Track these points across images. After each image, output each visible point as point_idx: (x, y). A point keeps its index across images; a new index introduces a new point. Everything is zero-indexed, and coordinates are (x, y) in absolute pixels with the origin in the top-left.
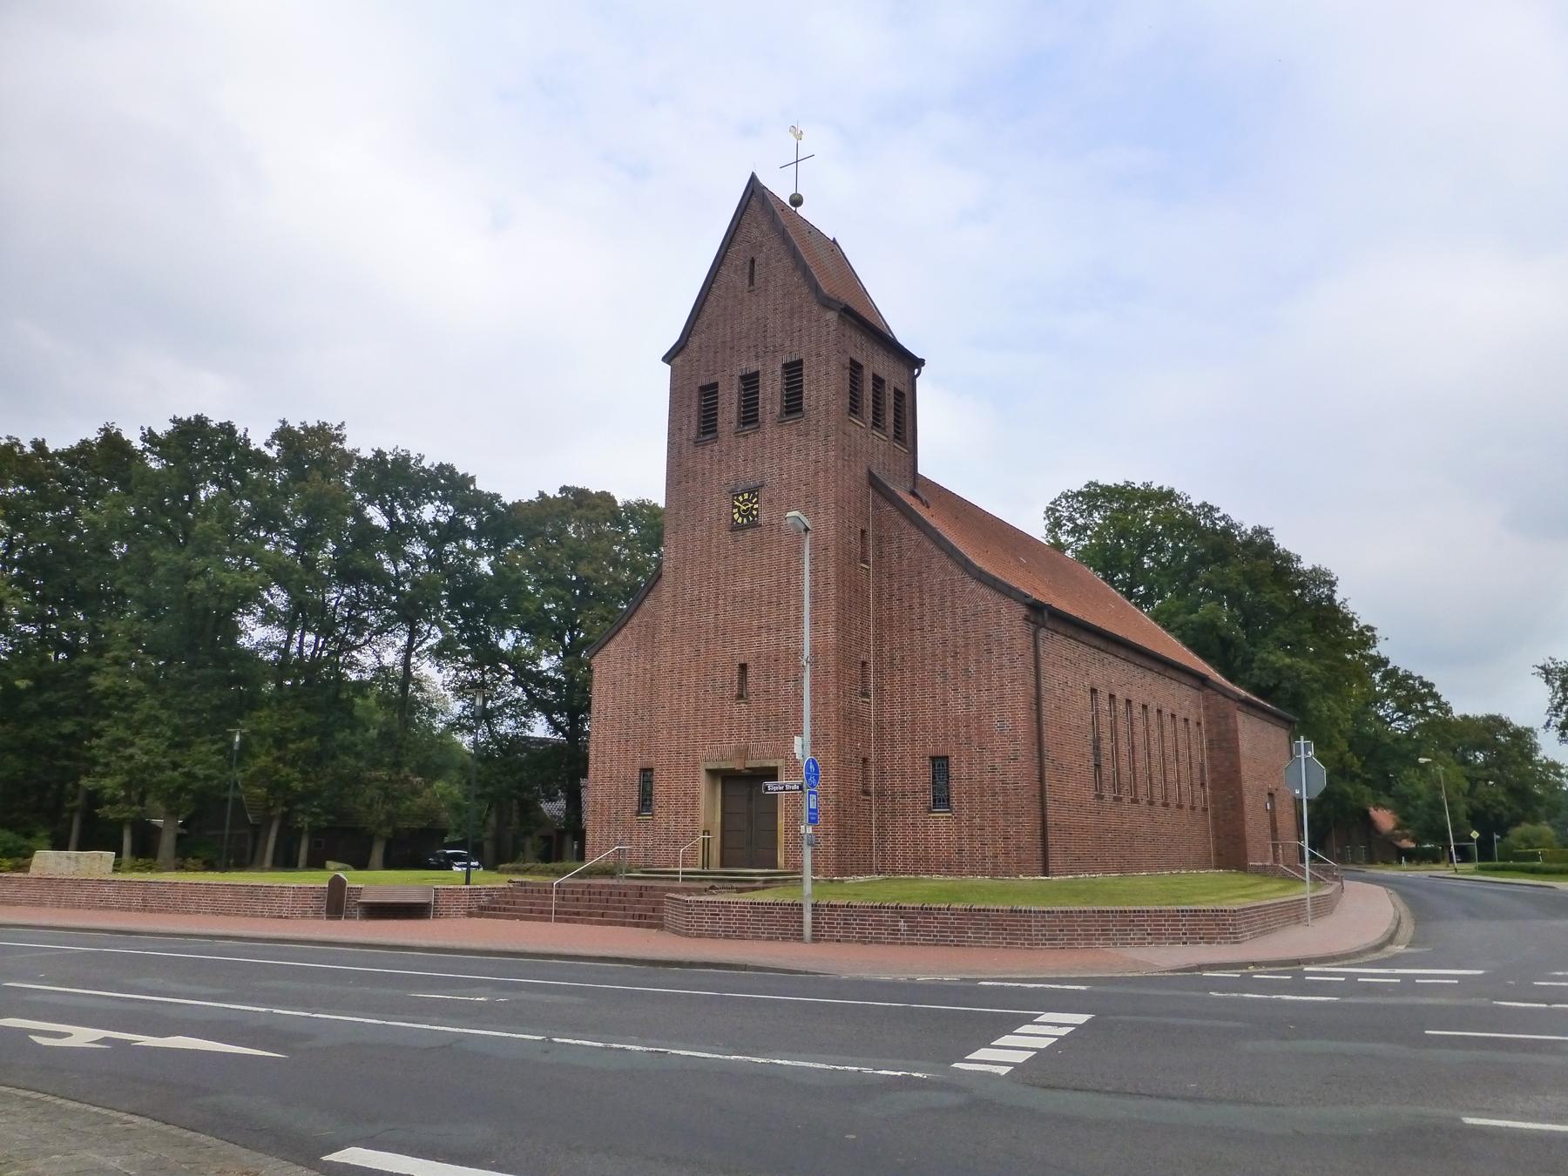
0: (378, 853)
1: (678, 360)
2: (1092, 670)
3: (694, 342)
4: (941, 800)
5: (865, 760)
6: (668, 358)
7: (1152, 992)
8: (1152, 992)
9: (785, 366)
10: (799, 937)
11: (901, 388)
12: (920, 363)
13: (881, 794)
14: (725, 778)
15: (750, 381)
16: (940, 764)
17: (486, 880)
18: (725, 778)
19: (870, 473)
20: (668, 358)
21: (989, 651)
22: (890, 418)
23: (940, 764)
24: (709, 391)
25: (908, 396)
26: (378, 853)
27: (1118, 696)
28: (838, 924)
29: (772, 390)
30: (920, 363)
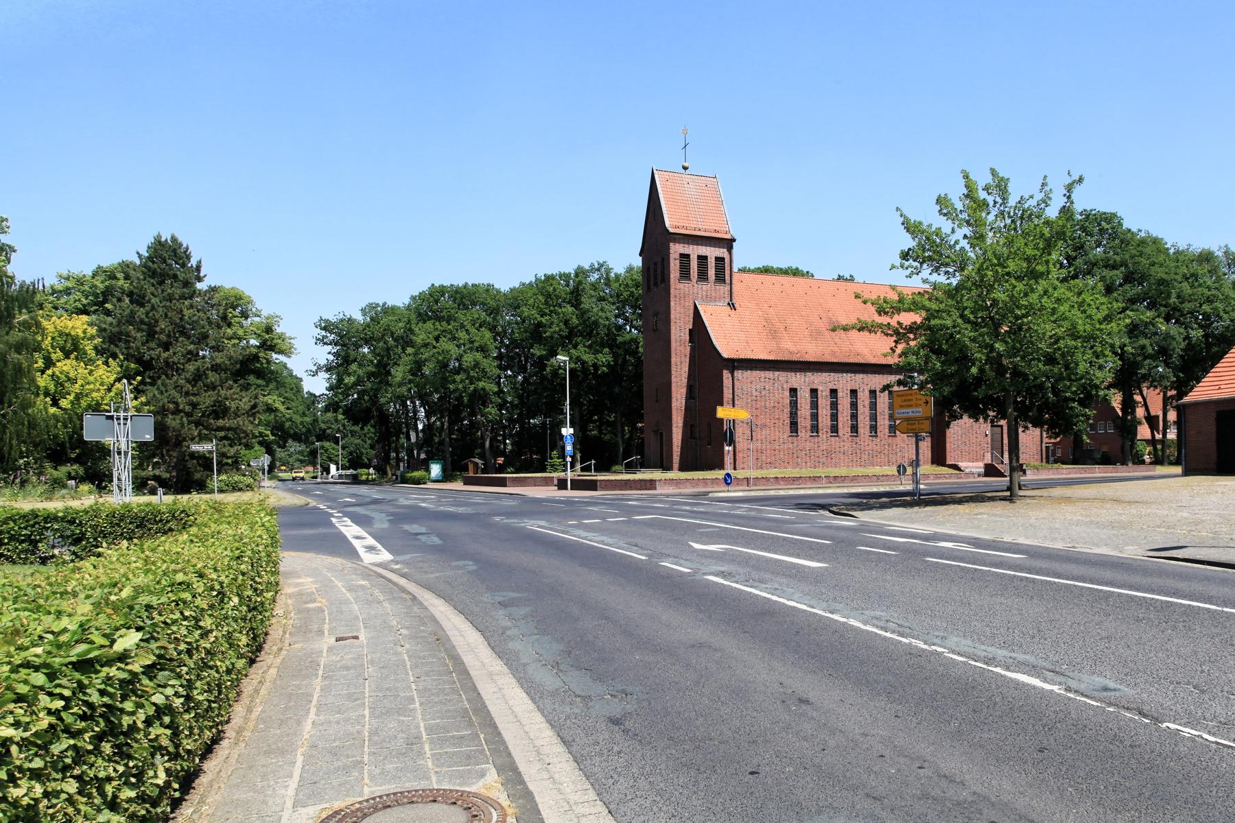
22: (712, 272)
25: (727, 261)
27: (820, 388)
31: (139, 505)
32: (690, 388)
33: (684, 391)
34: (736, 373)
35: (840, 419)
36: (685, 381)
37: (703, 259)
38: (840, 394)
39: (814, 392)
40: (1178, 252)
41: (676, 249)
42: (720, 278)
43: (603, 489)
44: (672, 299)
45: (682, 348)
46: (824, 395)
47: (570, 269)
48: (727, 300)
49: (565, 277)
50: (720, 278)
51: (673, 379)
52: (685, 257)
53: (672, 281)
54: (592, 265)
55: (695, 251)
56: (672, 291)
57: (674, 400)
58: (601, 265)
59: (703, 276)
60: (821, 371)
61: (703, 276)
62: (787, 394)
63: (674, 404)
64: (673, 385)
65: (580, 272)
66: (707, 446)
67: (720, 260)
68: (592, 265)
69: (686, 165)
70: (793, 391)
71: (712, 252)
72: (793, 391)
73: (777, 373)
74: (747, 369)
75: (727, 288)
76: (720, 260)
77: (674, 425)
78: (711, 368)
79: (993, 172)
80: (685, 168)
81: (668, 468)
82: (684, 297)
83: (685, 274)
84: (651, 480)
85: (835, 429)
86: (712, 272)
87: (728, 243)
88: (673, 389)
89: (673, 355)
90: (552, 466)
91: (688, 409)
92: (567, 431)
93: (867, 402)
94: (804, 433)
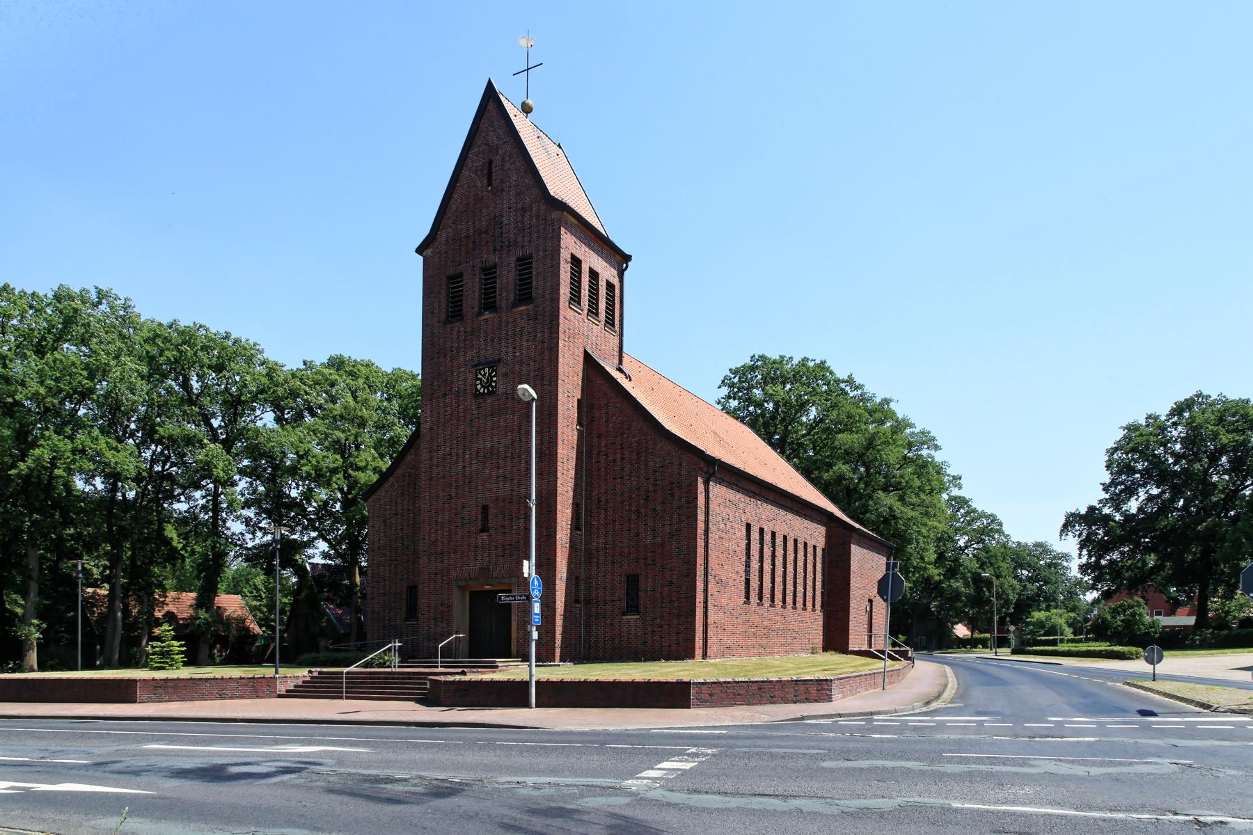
0: (33, 657)
1: (428, 252)
3: (442, 236)
4: (632, 608)
5: (577, 578)
6: (419, 250)
9: (519, 260)
10: (526, 704)
12: (628, 258)
13: (588, 602)
15: (489, 272)
16: (632, 582)
19: (586, 352)
20: (419, 250)
21: (672, 495)
23: (632, 582)
24: (456, 279)
26: (33, 657)
28: (555, 695)
29: (507, 277)
30: (628, 258)
32: (576, 506)
33: (569, 511)
36: (571, 494)
40: (863, 398)
41: (570, 244)
43: (704, 703)
44: (561, 336)
48: (616, 361)
50: (610, 322)
51: (559, 490)
52: (576, 262)
55: (592, 260)
57: (559, 528)
59: (593, 311)
60: (767, 500)
61: (593, 311)
67: (610, 286)
69: (530, 102)
70: (748, 526)
72: (748, 526)
73: (739, 495)
75: (617, 341)
77: (558, 576)
78: (644, 469)
79: (501, 242)
82: (577, 333)
83: (575, 298)
87: (620, 259)
88: (559, 507)
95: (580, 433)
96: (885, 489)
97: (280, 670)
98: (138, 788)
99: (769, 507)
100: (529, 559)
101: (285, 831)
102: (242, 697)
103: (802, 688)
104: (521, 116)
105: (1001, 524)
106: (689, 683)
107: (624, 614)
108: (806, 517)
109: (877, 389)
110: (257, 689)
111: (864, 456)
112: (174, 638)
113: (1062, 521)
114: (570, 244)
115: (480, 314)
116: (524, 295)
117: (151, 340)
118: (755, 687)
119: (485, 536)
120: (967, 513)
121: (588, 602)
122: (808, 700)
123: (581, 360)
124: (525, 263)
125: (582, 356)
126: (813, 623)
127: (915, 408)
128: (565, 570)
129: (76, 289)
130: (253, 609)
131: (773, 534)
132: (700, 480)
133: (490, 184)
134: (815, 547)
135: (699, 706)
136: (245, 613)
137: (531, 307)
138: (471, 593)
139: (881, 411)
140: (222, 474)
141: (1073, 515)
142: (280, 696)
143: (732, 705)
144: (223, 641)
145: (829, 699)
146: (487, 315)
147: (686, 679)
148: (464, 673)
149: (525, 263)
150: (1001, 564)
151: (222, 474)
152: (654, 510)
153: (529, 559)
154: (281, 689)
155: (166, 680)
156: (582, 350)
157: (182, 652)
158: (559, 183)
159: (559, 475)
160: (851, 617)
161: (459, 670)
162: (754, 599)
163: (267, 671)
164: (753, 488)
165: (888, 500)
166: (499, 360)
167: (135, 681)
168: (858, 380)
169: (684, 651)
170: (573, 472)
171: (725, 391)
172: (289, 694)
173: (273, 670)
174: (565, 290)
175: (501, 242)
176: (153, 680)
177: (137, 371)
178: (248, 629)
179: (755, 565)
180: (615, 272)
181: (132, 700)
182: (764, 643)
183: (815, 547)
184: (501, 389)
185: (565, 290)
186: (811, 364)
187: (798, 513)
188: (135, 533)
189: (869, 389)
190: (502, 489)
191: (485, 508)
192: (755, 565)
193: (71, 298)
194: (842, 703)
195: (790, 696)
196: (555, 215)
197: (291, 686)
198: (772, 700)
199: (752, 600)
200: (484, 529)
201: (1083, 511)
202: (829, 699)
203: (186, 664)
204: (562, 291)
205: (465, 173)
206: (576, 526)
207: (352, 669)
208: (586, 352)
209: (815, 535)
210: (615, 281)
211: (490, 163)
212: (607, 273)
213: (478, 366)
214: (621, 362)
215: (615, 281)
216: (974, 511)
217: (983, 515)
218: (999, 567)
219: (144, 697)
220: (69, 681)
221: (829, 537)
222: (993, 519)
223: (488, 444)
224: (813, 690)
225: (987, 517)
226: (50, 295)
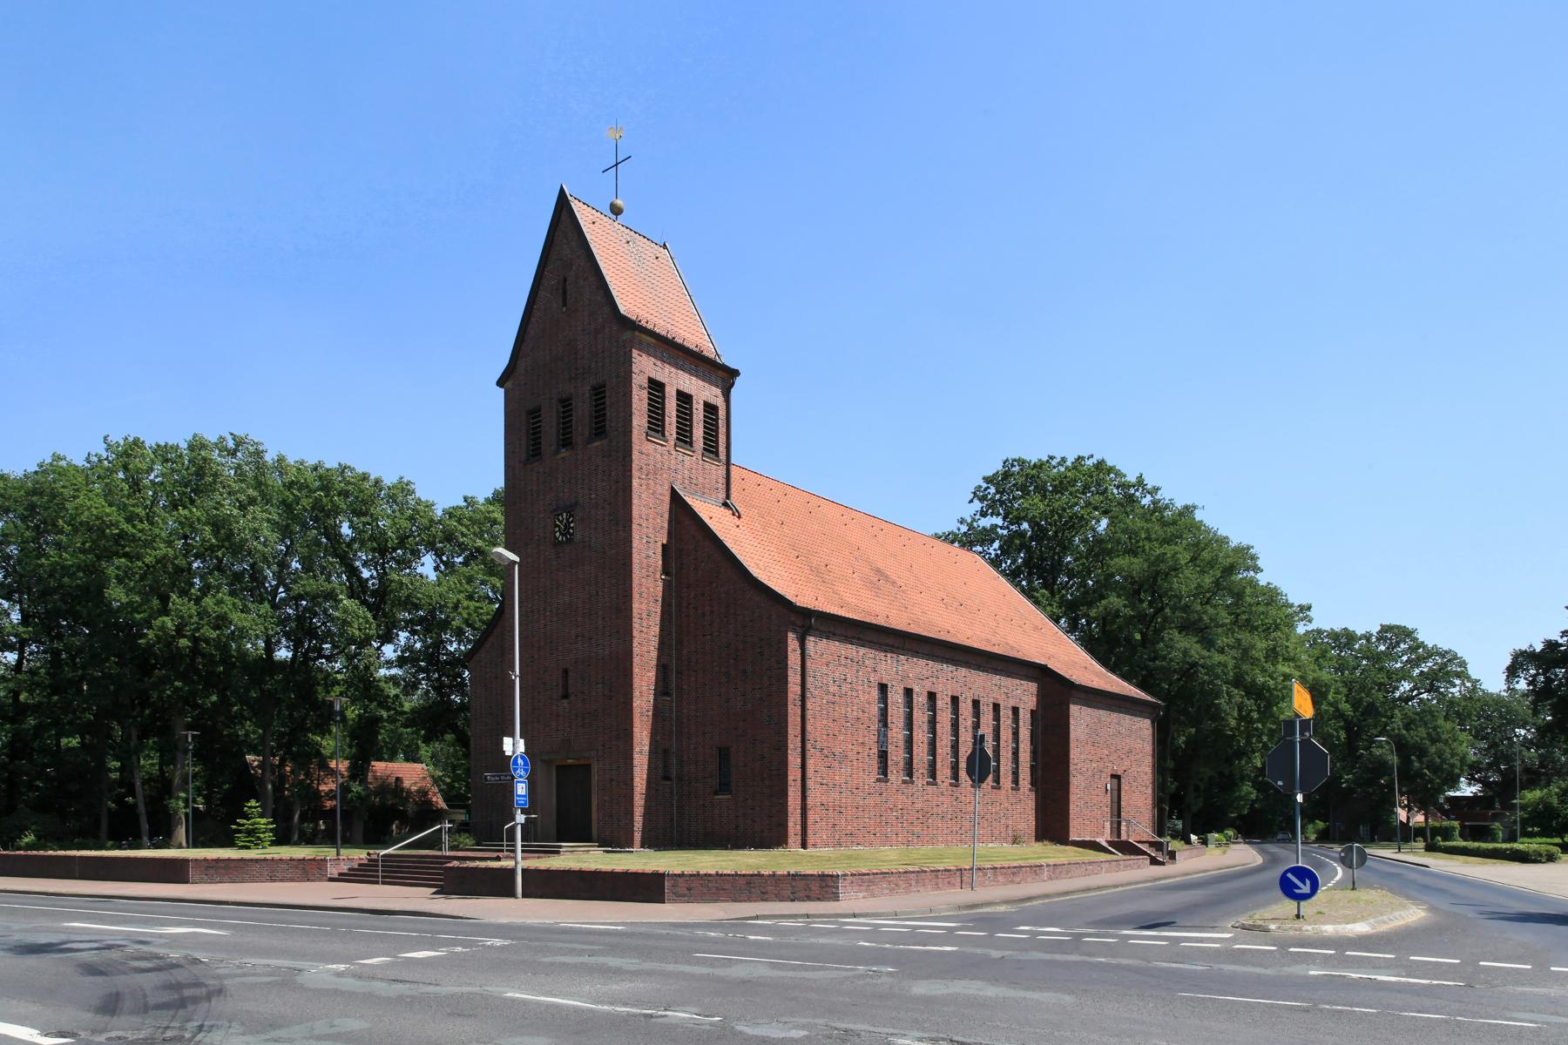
0: (181, 833)
1: (509, 384)
2: (883, 666)
3: (521, 364)
4: (724, 787)
5: (665, 751)
6: (500, 383)
7: (1229, 968)
8: (1229, 968)
9: (594, 389)
10: (512, 894)
11: (712, 401)
12: (735, 373)
13: (680, 779)
14: (1113, 776)
15: (566, 403)
16: (724, 755)
17: (359, 855)
18: (1113, 776)
19: (673, 492)
20: (500, 383)
21: (761, 654)
22: (698, 432)
23: (724, 755)
24: (535, 413)
25: (722, 413)
26: (181, 833)
27: (916, 689)
28: (546, 885)
29: (583, 409)
30: (735, 373)
31: (1412, 851)
32: (663, 669)
33: (652, 674)
34: (811, 642)
35: (939, 751)
36: (654, 654)
37: (684, 399)
38: (940, 704)
39: (909, 692)
40: (1157, 508)
41: (645, 366)
42: (711, 448)
43: (680, 897)
44: (635, 473)
45: (650, 583)
46: (920, 700)
47: (178, 436)
48: (722, 495)
49: (164, 453)
50: (711, 448)
51: (636, 650)
52: (656, 387)
53: (635, 432)
54: (222, 439)
55: (677, 380)
56: (635, 456)
57: (636, 693)
58: (239, 442)
59: (684, 437)
60: (916, 653)
61: (684, 437)
62: (875, 693)
63: (637, 703)
64: (636, 660)
65: (197, 445)
66: (731, 783)
67: (710, 409)
68: (222, 439)
69: (619, 202)
70: (883, 688)
71: (703, 392)
72: (883, 688)
73: (862, 650)
74: (830, 636)
75: (722, 471)
76: (710, 409)
79: (579, 369)
80: (616, 211)
81: (616, 840)
82: (658, 469)
83: (656, 425)
84: (823, 877)
85: (933, 773)
86: (698, 432)
87: (725, 376)
88: (636, 670)
89: (636, 596)
90: (250, 833)
91: (658, 715)
92: (513, 746)
93: (969, 723)
94: (896, 776)
95: (667, 586)
96: (1181, 629)
97: (343, 851)
98: (580, 997)
99: (922, 662)
100: (512, 735)
101: (517, 1040)
102: (292, 880)
103: (801, 884)
104: (606, 221)
105: (1463, 664)
106: (663, 874)
107: (716, 793)
108: (996, 671)
109: (1175, 491)
110: (308, 871)
111: (1151, 585)
112: (261, 816)
113: (1508, 661)
114: (645, 366)
115: (557, 452)
116: (599, 431)
117: (290, 486)
118: (742, 881)
119: (565, 702)
120: (1413, 649)
121: (680, 779)
122: (809, 898)
123: (667, 506)
124: (599, 391)
125: (667, 499)
126: (1022, 807)
127: (1226, 520)
128: (646, 741)
129: (212, 438)
130: (436, 780)
131: (932, 696)
132: (791, 636)
133: (565, 304)
134: (1015, 710)
135: (675, 901)
136: (428, 783)
137: (605, 442)
138: (558, 767)
139: (1180, 525)
140: (357, 633)
141: (1522, 653)
142: (331, 880)
143: (715, 901)
144: (403, 817)
145: (836, 898)
146: (564, 453)
147: (661, 870)
148: (498, 859)
149: (599, 391)
150: (1441, 722)
151: (357, 633)
152: (744, 672)
153: (512, 735)
154: (332, 871)
155: (218, 860)
156: (667, 487)
157: (271, 830)
158: (628, 303)
159: (635, 633)
160: (1072, 798)
161: (495, 855)
162: (896, 776)
163: (328, 852)
164: (890, 641)
165: (1182, 645)
166: (576, 504)
167: (186, 861)
168: (1150, 483)
169: (773, 837)
170: (657, 629)
171: (977, 505)
172: (342, 878)
173: (334, 850)
174: (640, 421)
175: (579, 369)
176: (205, 860)
177: (269, 521)
178: (429, 802)
179: (897, 733)
180: (718, 391)
181: (183, 880)
182: (917, 829)
183: (1015, 710)
184: (578, 537)
185: (640, 421)
186: (1090, 463)
187: (979, 668)
188: (294, 699)
189: (1164, 495)
190: (574, 654)
191: (566, 671)
192: (897, 733)
193: (203, 446)
194: (851, 900)
195: (788, 893)
196: (627, 335)
197: (344, 868)
198: (764, 897)
199: (939, 777)
200: (566, 696)
201: (1539, 647)
202: (835, 897)
203: (273, 843)
204: (635, 423)
205: (542, 293)
206: (662, 688)
207: (390, 851)
208: (673, 492)
209: (1024, 695)
210: (719, 402)
211: (565, 280)
212: (712, 394)
213: (556, 512)
214: (728, 497)
215: (719, 402)
216: (1422, 645)
217: (1432, 653)
218: (1435, 729)
219: (197, 878)
220: (128, 859)
221: (1041, 696)
222: (1450, 657)
223: (567, 599)
224: (815, 886)
225: (1443, 654)
226: (185, 445)
